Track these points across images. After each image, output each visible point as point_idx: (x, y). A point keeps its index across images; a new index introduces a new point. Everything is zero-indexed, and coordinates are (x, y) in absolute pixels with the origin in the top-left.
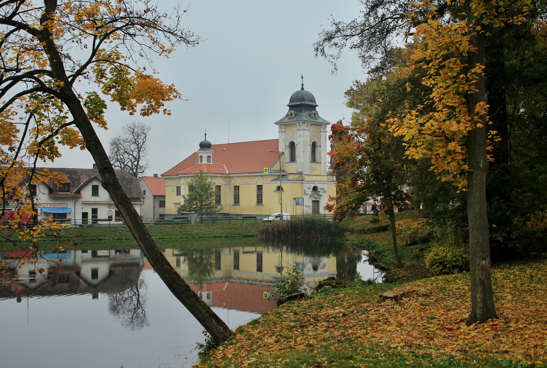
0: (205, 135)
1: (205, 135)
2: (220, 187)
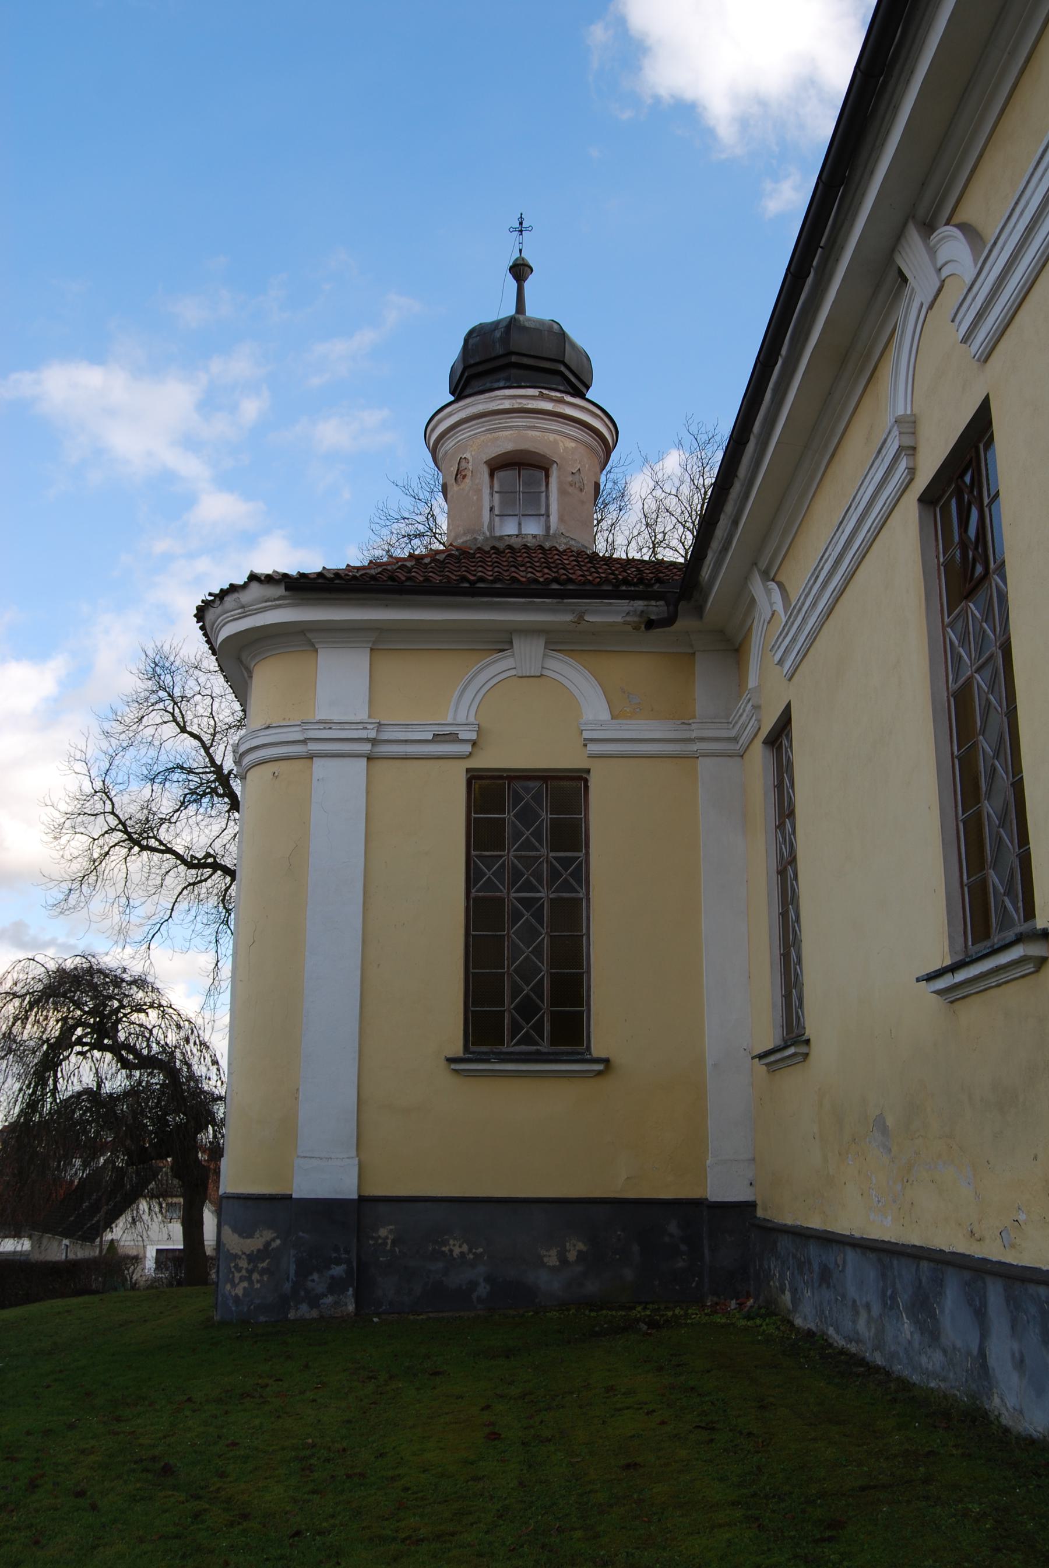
0: (520, 271)
1: (520, 271)
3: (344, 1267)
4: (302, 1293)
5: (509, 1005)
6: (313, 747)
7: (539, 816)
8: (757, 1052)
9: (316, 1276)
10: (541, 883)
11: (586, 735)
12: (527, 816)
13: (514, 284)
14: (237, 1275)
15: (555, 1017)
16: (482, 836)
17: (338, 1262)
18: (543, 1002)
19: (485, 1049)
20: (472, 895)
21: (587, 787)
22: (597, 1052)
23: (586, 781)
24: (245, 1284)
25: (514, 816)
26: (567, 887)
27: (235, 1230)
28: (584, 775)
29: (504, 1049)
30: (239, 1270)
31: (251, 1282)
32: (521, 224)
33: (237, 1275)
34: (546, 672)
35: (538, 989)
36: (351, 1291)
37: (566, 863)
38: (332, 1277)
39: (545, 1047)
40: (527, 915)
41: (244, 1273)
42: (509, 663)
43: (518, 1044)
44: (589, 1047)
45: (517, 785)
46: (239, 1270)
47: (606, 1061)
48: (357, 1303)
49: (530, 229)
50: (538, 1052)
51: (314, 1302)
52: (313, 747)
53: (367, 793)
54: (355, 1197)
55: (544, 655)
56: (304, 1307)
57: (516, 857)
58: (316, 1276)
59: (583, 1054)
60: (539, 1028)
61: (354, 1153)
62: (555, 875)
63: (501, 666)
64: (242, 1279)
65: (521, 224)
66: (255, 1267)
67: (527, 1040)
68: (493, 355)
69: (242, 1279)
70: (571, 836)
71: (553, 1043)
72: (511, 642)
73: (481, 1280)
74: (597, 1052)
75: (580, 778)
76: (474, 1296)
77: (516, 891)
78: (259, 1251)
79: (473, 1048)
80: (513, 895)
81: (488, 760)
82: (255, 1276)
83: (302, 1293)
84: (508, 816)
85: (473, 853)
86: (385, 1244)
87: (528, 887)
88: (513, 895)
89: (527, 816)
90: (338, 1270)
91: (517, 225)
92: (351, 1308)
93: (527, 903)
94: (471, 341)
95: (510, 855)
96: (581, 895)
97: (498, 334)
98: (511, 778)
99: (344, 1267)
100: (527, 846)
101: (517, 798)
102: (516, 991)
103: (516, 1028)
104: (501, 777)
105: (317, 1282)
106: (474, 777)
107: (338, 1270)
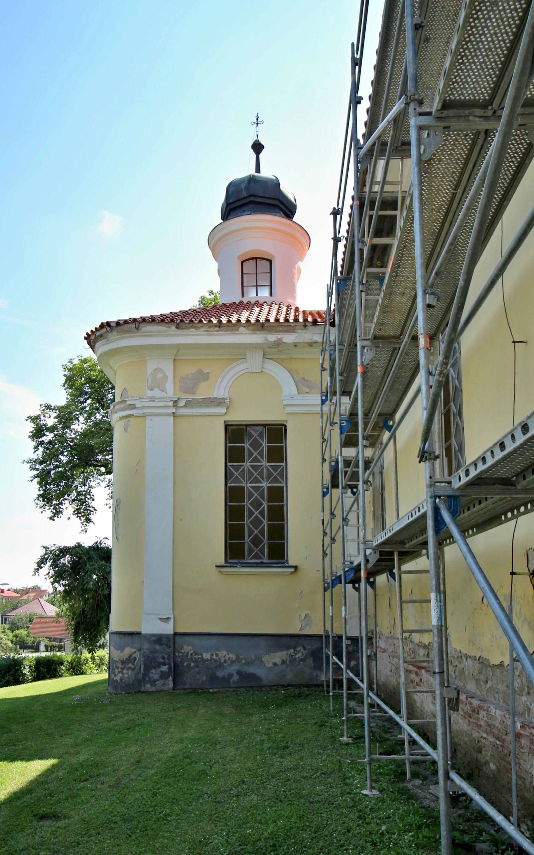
0: (258, 147)
1: (258, 147)
2: (276, 432)
3: (167, 666)
4: (147, 679)
5: (247, 540)
6: (146, 411)
7: (261, 445)
8: (218, 564)
9: (153, 671)
10: (263, 479)
11: (285, 403)
12: (256, 445)
13: (254, 155)
14: (117, 670)
15: (270, 546)
16: (233, 455)
17: (164, 664)
18: (264, 537)
19: (235, 561)
20: (229, 485)
21: (286, 430)
22: (291, 562)
23: (285, 426)
24: (120, 675)
25: (249, 445)
26: (276, 480)
27: (115, 648)
28: (285, 423)
29: (245, 561)
30: (117, 668)
31: (123, 674)
32: (257, 119)
33: (117, 670)
34: (264, 370)
35: (262, 532)
36: (171, 678)
37: (275, 468)
38: (162, 671)
39: (266, 560)
40: (256, 495)
41: (120, 670)
42: (242, 366)
43: (251, 559)
44: (287, 561)
45: (249, 429)
46: (117, 668)
47: (296, 568)
48: (174, 683)
49: (262, 122)
50: (262, 563)
51: (153, 683)
52: (146, 411)
53: (174, 434)
54: (172, 633)
55: (263, 361)
56: (148, 686)
57: (251, 466)
58: (153, 671)
59: (284, 563)
60: (262, 551)
61: (171, 612)
62: (270, 474)
63: (240, 368)
64: (119, 672)
65: (257, 119)
66: (125, 666)
67: (256, 557)
68: (242, 197)
69: (119, 672)
70: (278, 454)
71: (270, 558)
72: (246, 354)
73: (234, 673)
74: (291, 562)
75: (282, 425)
76: (231, 681)
77: (250, 483)
78: (126, 659)
79: (230, 561)
80: (249, 485)
81: (240, 415)
82: (125, 671)
83: (147, 679)
84: (246, 445)
85: (229, 464)
86: (187, 655)
87: (256, 480)
88: (249, 485)
89: (256, 445)
90: (164, 668)
91: (255, 121)
92: (171, 685)
93: (256, 489)
94: (230, 189)
95: (247, 464)
96: (283, 484)
97: (243, 186)
98: (247, 425)
99: (167, 666)
100: (256, 460)
101: (250, 436)
102: (251, 532)
103: (251, 551)
104: (242, 425)
105: (155, 674)
106: (227, 426)
107: (164, 668)
